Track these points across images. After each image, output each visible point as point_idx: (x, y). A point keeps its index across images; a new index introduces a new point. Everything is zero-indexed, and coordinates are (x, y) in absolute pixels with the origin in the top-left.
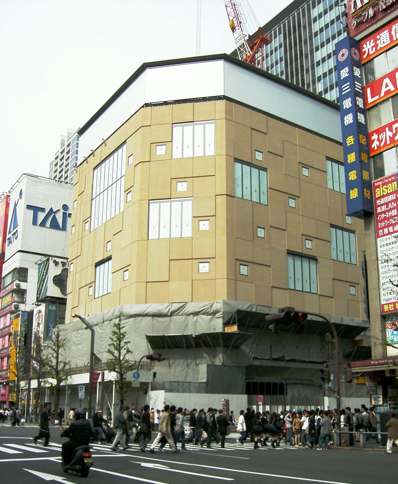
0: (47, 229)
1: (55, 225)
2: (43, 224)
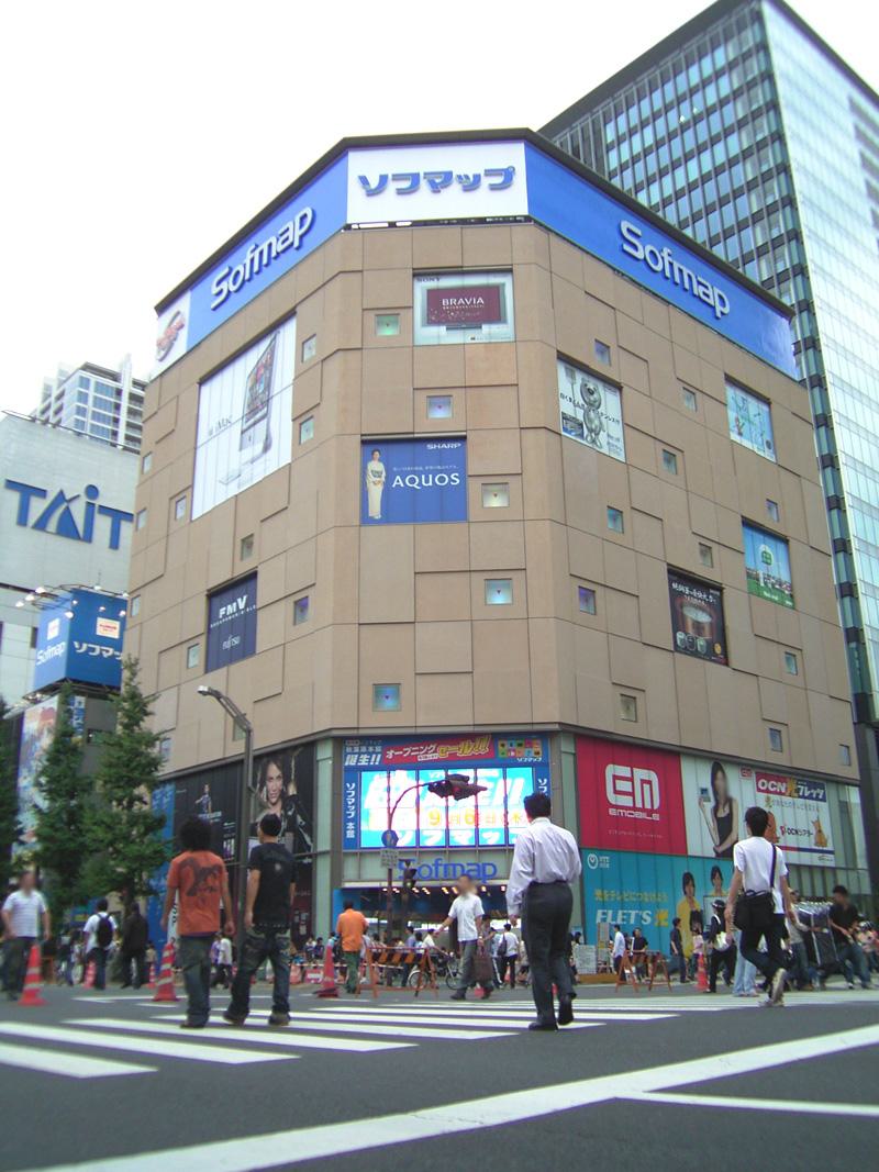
0: (49, 536)
1: (67, 529)
2: (41, 525)
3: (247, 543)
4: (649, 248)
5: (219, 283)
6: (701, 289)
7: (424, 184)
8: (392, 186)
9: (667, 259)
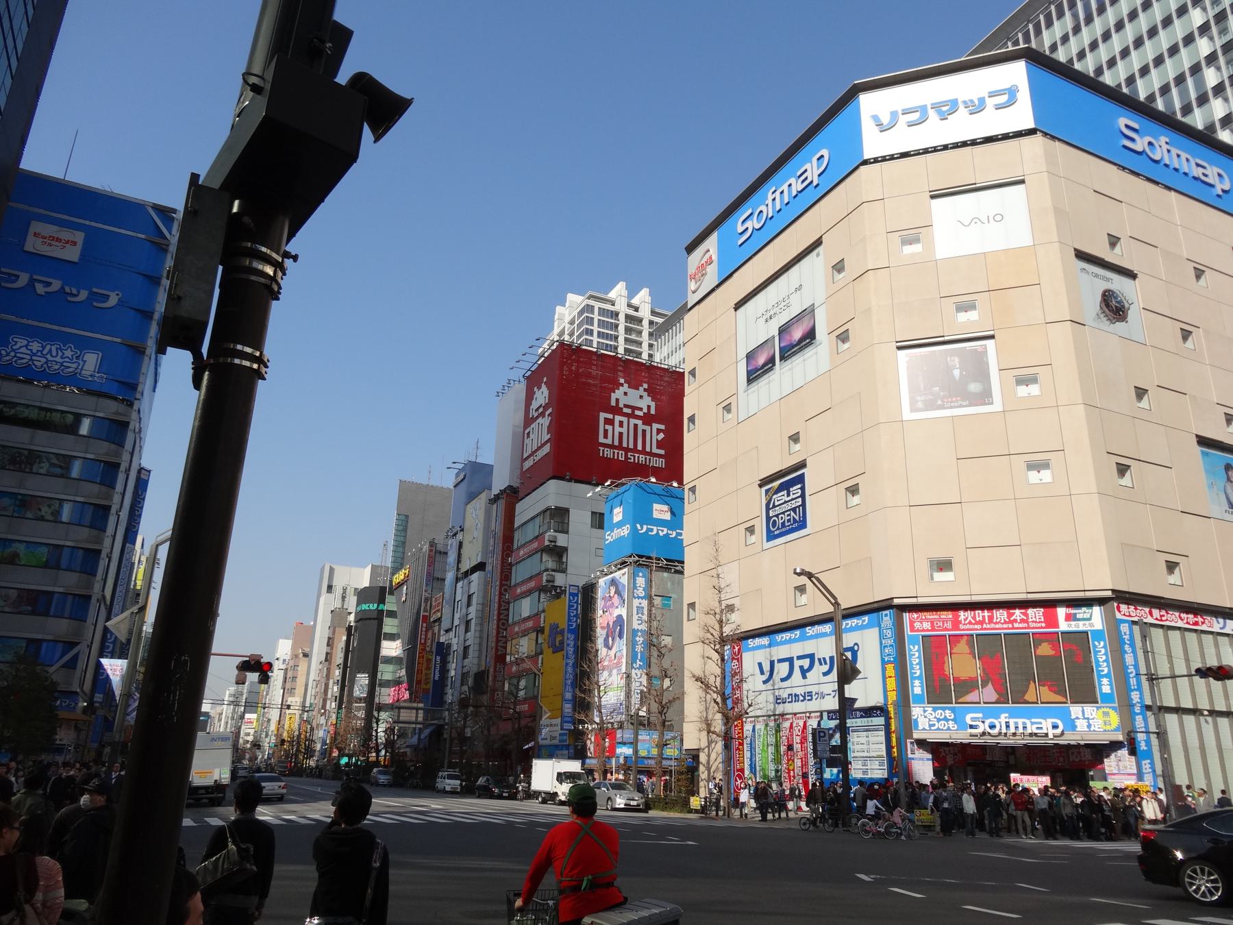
3: (795, 438)
4: (1148, 139)
5: (744, 222)
6: (1201, 170)
7: (932, 114)
8: (904, 119)
9: (1165, 147)
